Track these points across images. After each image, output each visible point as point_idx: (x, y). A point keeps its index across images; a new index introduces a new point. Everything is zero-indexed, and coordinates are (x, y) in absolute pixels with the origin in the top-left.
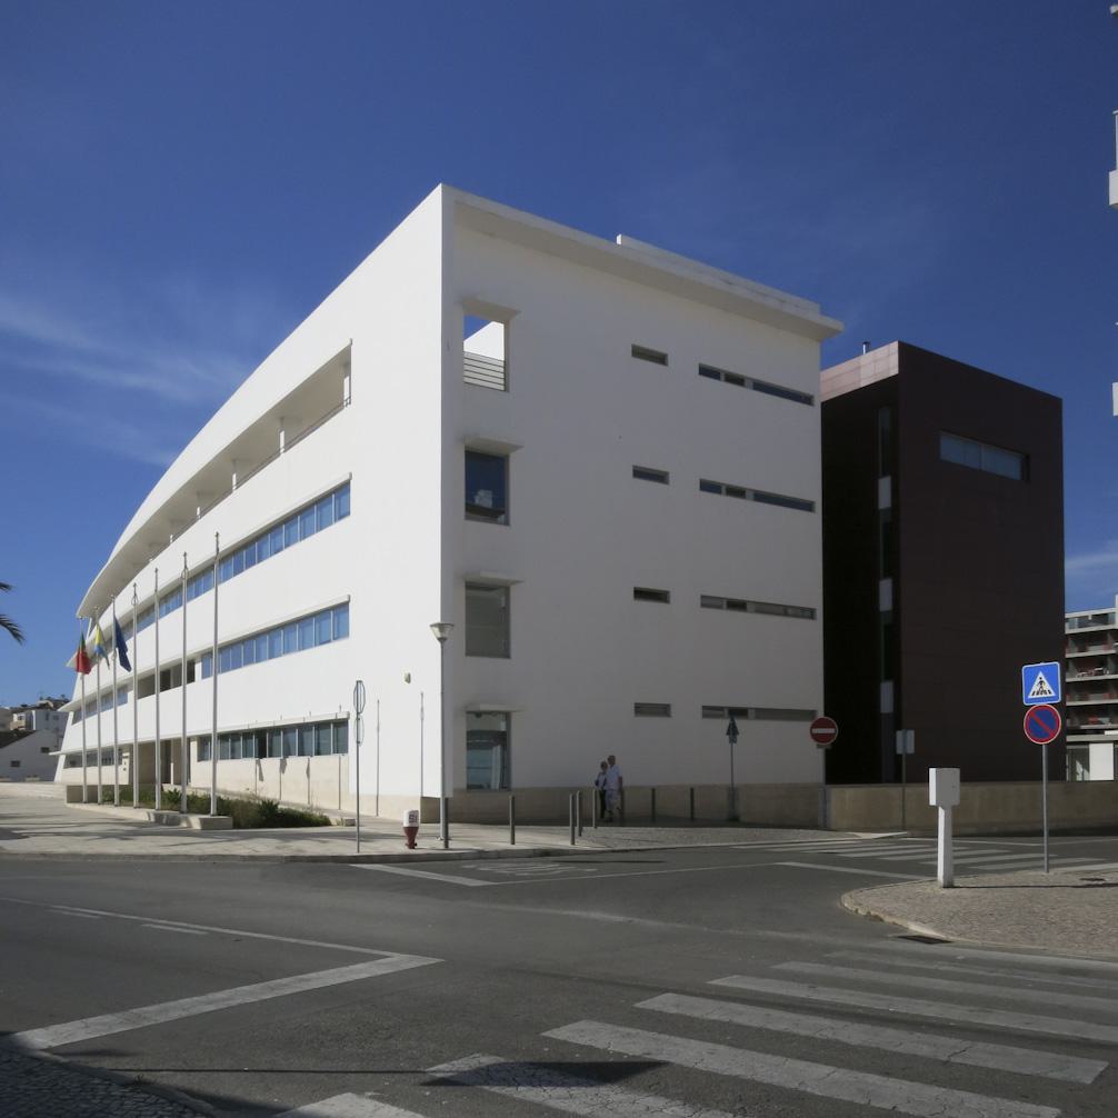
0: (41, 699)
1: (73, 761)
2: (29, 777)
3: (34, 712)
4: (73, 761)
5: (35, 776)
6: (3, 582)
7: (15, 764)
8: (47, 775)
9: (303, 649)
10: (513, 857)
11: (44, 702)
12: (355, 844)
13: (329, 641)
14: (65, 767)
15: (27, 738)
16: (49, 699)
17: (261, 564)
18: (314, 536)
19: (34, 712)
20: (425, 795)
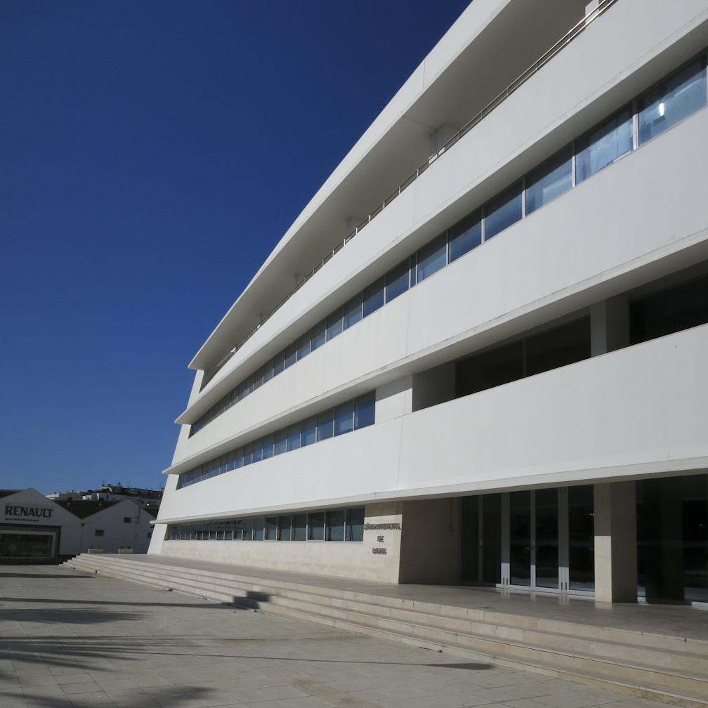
0: (103, 486)
1: (178, 531)
2: (122, 548)
3: (98, 495)
4: (178, 531)
5: (129, 548)
6: (6, 488)
7: (99, 533)
8: (140, 545)
9: (291, 450)
10: (369, 627)
11: (105, 488)
12: (459, 642)
13: (351, 430)
14: (168, 538)
15: (115, 506)
16: (109, 485)
17: (266, 384)
18: (272, 380)
19: (98, 495)
20: (395, 578)
